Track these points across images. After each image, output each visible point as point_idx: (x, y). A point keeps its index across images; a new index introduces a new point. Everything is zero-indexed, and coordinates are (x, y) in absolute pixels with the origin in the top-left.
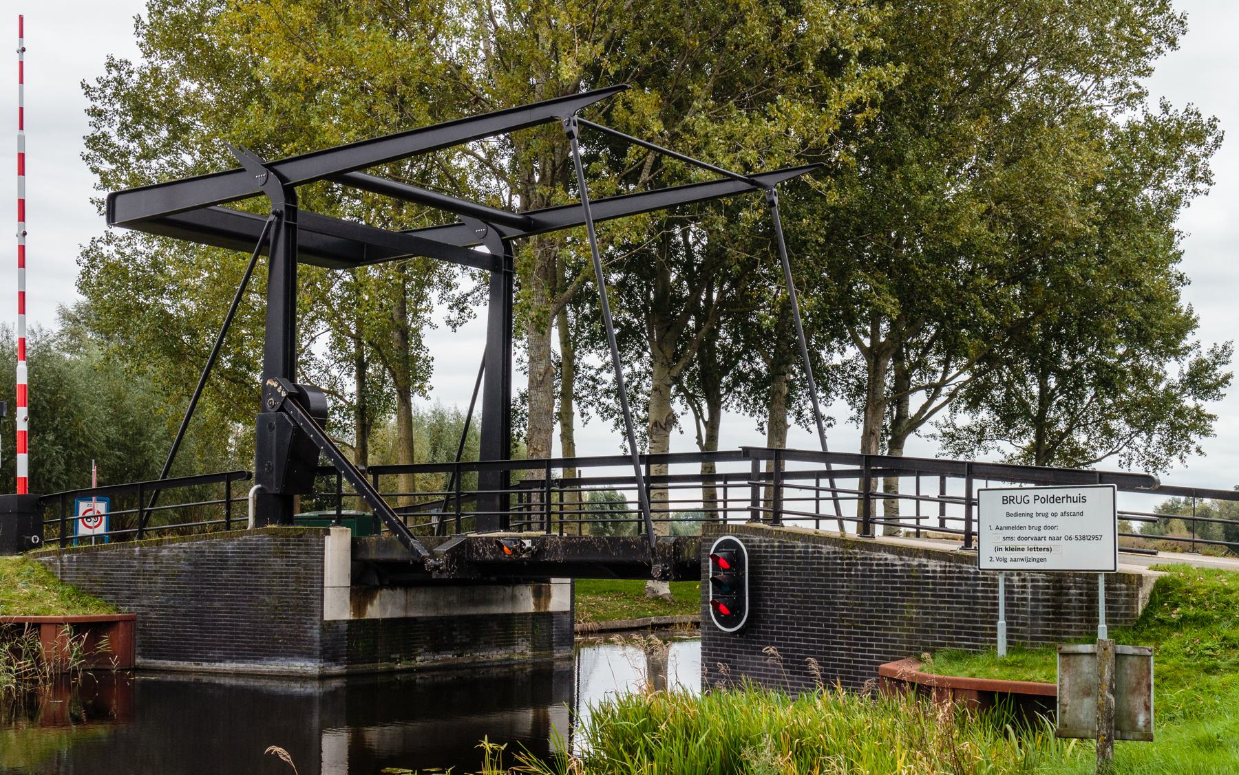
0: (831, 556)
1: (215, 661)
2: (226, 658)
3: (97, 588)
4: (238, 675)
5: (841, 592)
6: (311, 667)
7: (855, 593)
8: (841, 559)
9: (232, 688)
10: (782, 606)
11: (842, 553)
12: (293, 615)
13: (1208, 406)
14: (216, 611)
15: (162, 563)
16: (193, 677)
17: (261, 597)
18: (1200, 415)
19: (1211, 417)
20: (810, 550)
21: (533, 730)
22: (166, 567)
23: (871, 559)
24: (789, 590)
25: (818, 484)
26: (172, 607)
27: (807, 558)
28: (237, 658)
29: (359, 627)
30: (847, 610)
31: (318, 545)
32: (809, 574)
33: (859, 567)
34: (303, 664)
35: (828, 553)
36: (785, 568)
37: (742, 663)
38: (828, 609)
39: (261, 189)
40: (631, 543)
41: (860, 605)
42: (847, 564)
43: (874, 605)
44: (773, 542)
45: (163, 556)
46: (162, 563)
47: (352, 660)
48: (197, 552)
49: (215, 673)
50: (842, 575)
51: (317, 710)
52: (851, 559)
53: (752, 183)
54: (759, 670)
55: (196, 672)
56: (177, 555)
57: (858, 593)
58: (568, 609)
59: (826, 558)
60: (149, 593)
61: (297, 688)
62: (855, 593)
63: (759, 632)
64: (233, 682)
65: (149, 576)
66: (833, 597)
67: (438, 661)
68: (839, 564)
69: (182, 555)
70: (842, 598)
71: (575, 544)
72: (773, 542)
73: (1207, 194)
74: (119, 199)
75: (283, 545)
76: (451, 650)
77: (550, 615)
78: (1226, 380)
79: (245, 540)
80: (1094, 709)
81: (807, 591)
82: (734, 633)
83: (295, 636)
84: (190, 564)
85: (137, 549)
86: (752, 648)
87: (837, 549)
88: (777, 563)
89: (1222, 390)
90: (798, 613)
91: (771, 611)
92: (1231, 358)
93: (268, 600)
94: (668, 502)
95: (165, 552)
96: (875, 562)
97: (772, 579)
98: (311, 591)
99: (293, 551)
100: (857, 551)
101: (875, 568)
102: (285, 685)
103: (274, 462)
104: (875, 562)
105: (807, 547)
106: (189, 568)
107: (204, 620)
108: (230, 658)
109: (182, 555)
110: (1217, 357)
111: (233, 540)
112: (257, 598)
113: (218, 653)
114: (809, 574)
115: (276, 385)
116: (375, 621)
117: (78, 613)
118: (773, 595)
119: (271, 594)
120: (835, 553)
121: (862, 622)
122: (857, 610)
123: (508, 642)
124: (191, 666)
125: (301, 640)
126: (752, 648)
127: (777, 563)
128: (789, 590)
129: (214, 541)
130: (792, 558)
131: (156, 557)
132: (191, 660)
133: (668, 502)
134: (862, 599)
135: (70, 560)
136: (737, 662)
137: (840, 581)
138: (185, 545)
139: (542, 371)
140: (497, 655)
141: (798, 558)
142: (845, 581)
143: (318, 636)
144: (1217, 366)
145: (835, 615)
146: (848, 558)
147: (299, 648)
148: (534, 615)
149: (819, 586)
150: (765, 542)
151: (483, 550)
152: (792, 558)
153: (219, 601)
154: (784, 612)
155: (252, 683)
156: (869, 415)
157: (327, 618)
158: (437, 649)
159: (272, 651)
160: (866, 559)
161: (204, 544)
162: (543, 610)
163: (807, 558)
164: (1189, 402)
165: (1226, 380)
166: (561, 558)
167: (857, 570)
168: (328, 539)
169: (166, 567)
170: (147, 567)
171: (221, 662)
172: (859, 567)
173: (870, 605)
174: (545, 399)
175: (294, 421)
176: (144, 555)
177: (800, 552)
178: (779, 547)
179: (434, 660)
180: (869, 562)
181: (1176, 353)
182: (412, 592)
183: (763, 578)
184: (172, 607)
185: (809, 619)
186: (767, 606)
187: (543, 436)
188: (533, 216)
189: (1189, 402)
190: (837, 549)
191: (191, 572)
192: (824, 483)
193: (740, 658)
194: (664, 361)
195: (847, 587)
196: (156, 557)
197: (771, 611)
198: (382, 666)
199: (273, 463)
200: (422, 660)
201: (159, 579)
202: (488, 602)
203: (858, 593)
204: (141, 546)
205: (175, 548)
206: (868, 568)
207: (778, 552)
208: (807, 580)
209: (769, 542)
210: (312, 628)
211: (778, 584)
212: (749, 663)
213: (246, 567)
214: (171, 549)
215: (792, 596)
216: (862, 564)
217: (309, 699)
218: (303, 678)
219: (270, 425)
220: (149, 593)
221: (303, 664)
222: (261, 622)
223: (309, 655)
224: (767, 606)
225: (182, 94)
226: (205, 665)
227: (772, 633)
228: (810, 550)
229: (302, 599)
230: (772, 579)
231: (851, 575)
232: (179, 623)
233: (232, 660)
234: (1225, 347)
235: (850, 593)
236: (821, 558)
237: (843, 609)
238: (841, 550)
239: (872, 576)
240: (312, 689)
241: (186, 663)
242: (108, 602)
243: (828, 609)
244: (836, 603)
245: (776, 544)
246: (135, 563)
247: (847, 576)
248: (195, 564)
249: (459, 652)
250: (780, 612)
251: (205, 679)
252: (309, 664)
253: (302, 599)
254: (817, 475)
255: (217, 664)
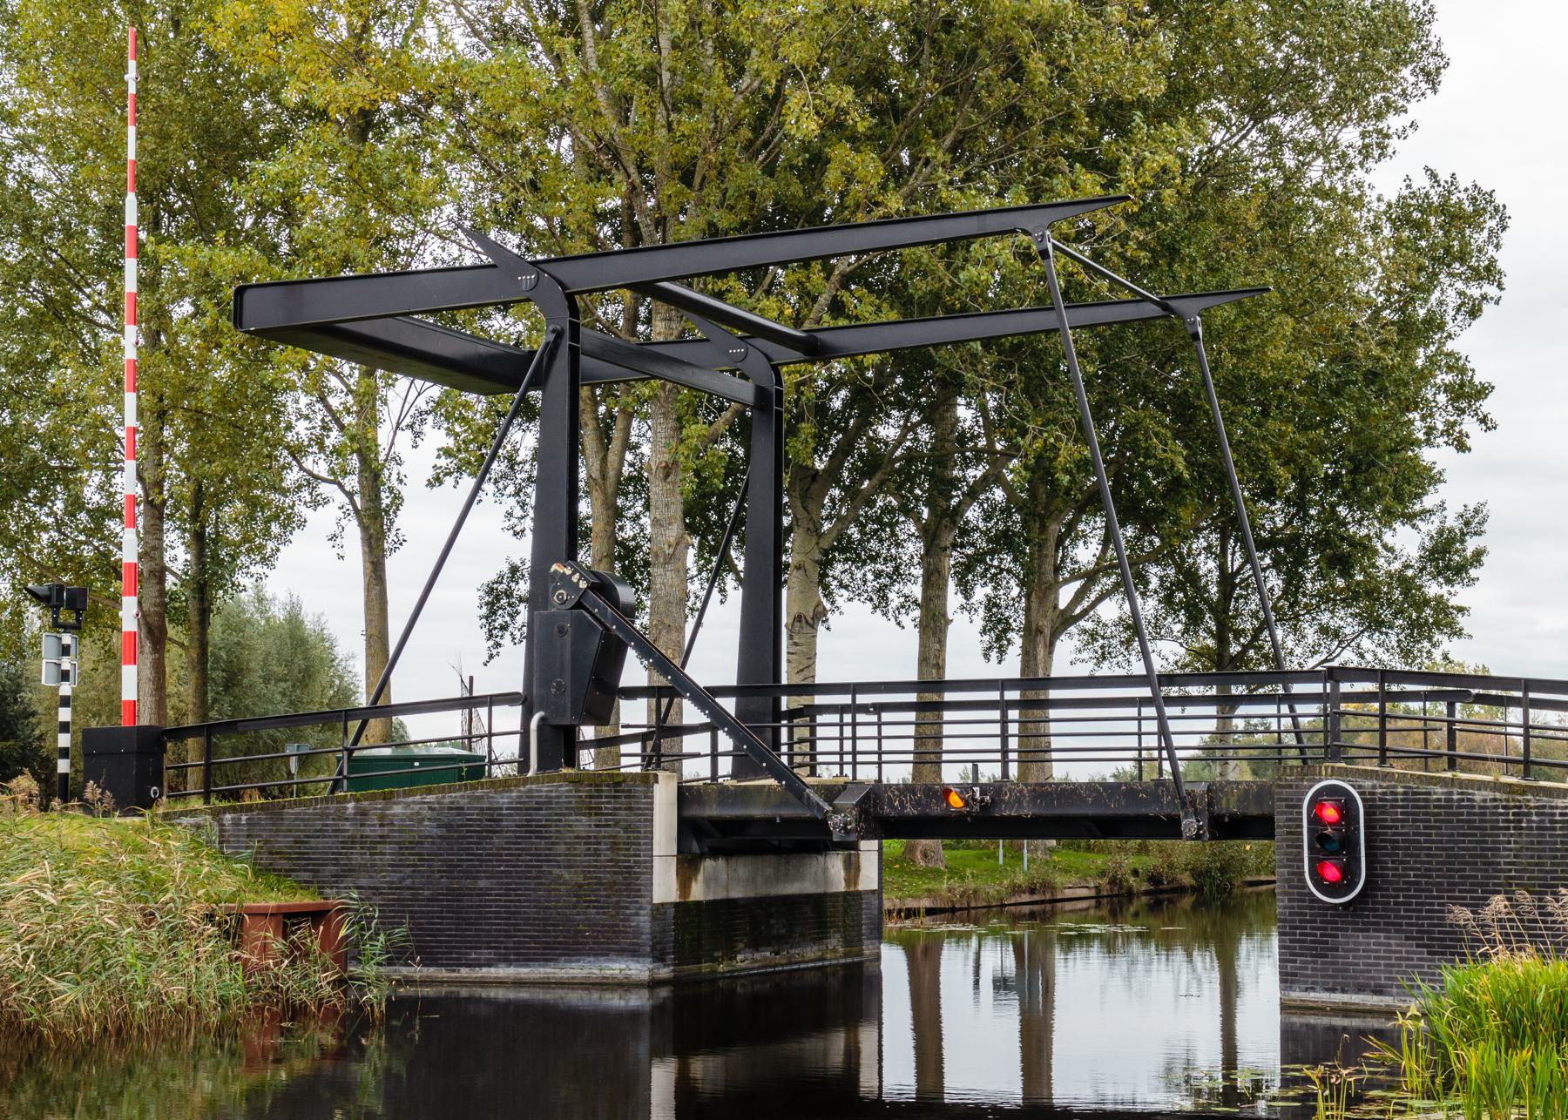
0: (1489, 804)
1: (481, 966)
2: (499, 960)
3: (284, 864)
4: (519, 983)
5: (1505, 849)
6: (639, 969)
7: (1527, 849)
8: (1504, 807)
9: (508, 1004)
10: (1412, 869)
11: (1507, 800)
12: (608, 896)
13: (1459, 595)
14: (482, 893)
15: (392, 825)
16: (444, 990)
17: (556, 871)
18: (1441, 606)
19: (1461, 610)
20: (1455, 797)
21: (844, 1062)
22: (399, 831)
23: (1552, 807)
24: (1423, 849)
25: (1279, 711)
26: (409, 888)
27: (1451, 807)
28: (516, 960)
29: (684, 910)
30: (1516, 871)
31: (646, 797)
32: (1454, 828)
33: (1534, 818)
34: (623, 966)
35: (1485, 801)
36: (1414, 821)
37: (1348, 943)
38: (1487, 871)
39: (528, 295)
40: (1138, 792)
41: (1536, 864)
42: (1514, 814)
43: (1558, 865)
44: (1395, 787)
45: (394, 815)
46: (392, 825)
47: (680, 960)
48: (451, 809)
49: (484, 983)
50: (1508, 828)
51: (645, 1031)
52: (1520, 807)
53: (1166, 308)
54: (1377, 951)
55: (451, 982)
56: (418, 813)
57: (1533, 849)
58: (876, 887)
59: (1480, 807)
60: (372, 869)
61: (615, 1001)
62: (1527, 849)
63: (1374, 903)
64: (511, 994)
65: (371, 845)
66: (1493, 856)
67: (756, 961)
68: (1501, 814)
69: (426, 813)
70: (1508, 856)
71: (1050, 793)
72: (1395, 787)
73: (1497, 303)
74: (248, 295)
75: (591, 797)
76: (769, 944)
77: (859, 894)
78: (1478, 555)
79: (530, 791)
80: (1162, 1069)
81: (1452, 849)
82: (1345, 905)
83: (612, 926)
84: (439, 826)
85: (351, 805)
86: (1363, 923)
87: (1498, 795)
88: (1402, 814)
89: (1473, 572)
90: (1437, 876)
91: (1393, 875)
92: (1486, 527)
93: (567, 876)
94: (1049, 735)
95: (397, 809)
96: (1558, 811)
97: (1395, 834)
98: (635, 862)
99: (607, 807)
100: (1529, 797)
101: (1558, 818)
102: (595, 996)
103: (569, 682)
104: (1558, 811)
105: (1451, 793)
106: (438, 832)
107: (463, 907)
108: (506, 960)
109: (426, 813)
110: (1467, 524)
111: (512, 791)
112: (550, 873)
113: (485, 954)
114: (1454, 828)
115: (568, 571)
116: (698, 903)
117: (274, 900)
118: (1397, 855)
119: (571, 867)
120: (1495, 800)
121: (1540, 886)
122: (1533, 871)
123: (821, 935)
124: (443, 973)
125: (619, 932)
126: (1363, 923)
127: (1402, 814)
128: (1423, 849)
129: (479, 793)
130: (1428, 807)
131: (382, 817)
132: (442, 965)
133: (1049, 735)
134: (1539, 857)
135: (236, 823)
136: (1339, 943)
137: (1504, 835)
138: (431, 798)
139: (672, 540)
140: (811, 952)
141: (1435, 807)
142: (1512, 835)
143: (648, 925)
144: (1467, 538)
145: (1499, 878)
146: (1515, 807)
147: (617, 944)
148: (846, 894)
149: (1470, 842)
150: (1381, 787)
151: (901, 802)
152: (1428, 807)
153: (487, 878)
154: (1415, 876)
155: (541, 995)
156: (1034, 605)
157: (656, 901)
158: (755, 945)
159: (574, 948)
160: (1544, 807)
161: (463, 797)
162: (852, 889)
163: (1451, 807)
164: (1433, 589)
165: (1478, 555)
166: (1027, 811)
167: (1529, 821)
168: (656, 787)
169: (399, 831)
170: (367, 831)
171: (490, 966)
172: (1534, 818)
173: (1553, 864)
174: (676, 581)
175: (602, 624)
176: (362, 813)
177: (1439, 800)
178: (1405, 793)
179: (754, 961)
180: (1548, 811)
181: (1409, 518)
182: (733, 861)
183: (1379, 834)
184: (409, 888)
185: (1456, 884)
186: (1387, 869)
187: (674, 636)
188: (818, 335)
189: (1433, 589)
190: (1498, 795)
191: (440, 837)
192: (1150, 711)
193: (1343, 936)
194: (811, 526)
195: (1515, 842)
196: (382, 817)
197: (1393, 875)
198: (706, 967)
199: (566, 681)
200: (744, 960)
201: (388, 848)
202: (788, 878)
203: (1533, 849)
204: (357, 800)
205: (414, 803)
206: (1547, 818)
207: (1402, 800)
208: (1452, 835)
209: (1387, 787)
210: (637, 914)
211: (1404, 841)
212: (1360, 944)
213: (530, 829)
214: (408, 804)
215: (1427, 855)
216: (1537, 814)
217: (633, 1016)
218: (625, 985)
219: (562, 631)
220: (372, 869)
221: (623, 966)
222: (556, 908)
223: (634, 953)
224: (1387, 869)
225: (1218, 321)
226: (464, 972)
227: (1396, 903)
228: (1455, 797)
229: (622, 873)
230: (1395, 834)
231: (1522, 828)
232: (421, 912)
233: (508, 962)
234: (1477, 511)
235: (1521, 849)
236: (1474, 807)
237: (1510, 871)
238: (1504, 796)
239: (1554, 829)
240: (638, 1000)
241: (432, 969)
242: (305, 885)
243: (1487, 871)
244: (1499, 863)
245: (1400, 790)
246: (348, 826)
247: (1515, 828)
248: (449, 826)
249: (776, 948)
250: (1409, 876)
251: (464, 992)
252: (633, 965)
253: (622, 873)
254: (1141, 702)
255: (485, 970)
